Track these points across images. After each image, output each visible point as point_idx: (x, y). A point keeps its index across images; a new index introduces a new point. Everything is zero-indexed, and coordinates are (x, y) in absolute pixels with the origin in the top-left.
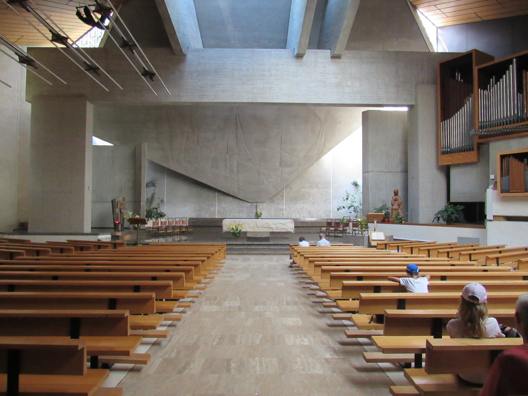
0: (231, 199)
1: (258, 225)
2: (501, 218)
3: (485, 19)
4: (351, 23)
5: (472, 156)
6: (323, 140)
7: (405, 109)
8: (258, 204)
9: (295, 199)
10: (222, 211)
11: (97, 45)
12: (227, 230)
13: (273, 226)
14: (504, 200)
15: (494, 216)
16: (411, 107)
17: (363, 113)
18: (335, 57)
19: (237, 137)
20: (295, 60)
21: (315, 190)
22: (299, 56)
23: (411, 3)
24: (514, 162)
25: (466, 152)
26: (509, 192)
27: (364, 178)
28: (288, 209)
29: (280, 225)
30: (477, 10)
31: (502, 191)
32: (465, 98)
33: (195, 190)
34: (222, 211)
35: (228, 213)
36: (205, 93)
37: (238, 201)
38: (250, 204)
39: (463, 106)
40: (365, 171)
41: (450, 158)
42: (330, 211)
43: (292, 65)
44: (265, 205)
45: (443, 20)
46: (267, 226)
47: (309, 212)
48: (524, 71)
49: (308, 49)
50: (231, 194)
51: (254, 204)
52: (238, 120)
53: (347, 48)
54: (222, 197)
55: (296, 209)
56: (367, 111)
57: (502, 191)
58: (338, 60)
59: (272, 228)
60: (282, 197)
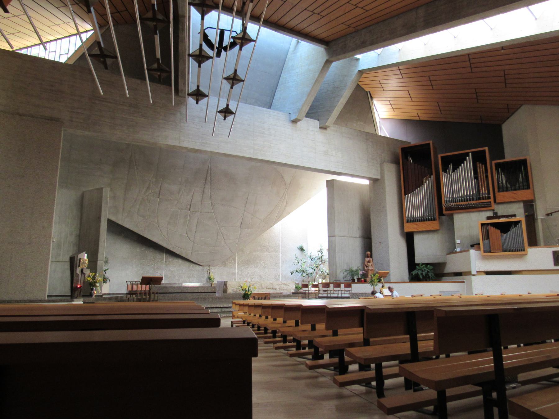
0: (180, 261)
1: (263, 285)
2: (483, 273)
3: (421, 119)
4: (345, 102)
5: (434, 225)
6: (285, 203)
7: (366, 182)
8: (211, 267)
9: (247, 263)
10: (169, 275)
11: (63, 60)
12: (232, 292)
13: (277, 287)
14: (484, 258)
15: (477, 272)
16: (374, 181)
17: (328, 182)
18: (323, 128)
19: (203, 192)
20: (291, 124)
21: (266, 253)
22: (295, 122)
23: (370, 95)
24: (492, 230)
25: (425, 222)
26: (490, 252)
27: (330, 243)
28: (240, 273)
29: (283, 286)
30: (419, 111)
31: (485, 252)
32: (423, 178)
33: (138, 250)
34: (169, 275)
35: (177, 278)
36: (208, 142)
37: (187, 264)
38: (201, 268)
39: (422, 184)
40: (331, 235)
41: (415, 226)
42: (279, 276)
43: (288, 129)
44: (217, 268)
45: (388, 113)
46: (271, 287)
47: (260, 276)
48: (478, 163)
49: (306, 117)
50: (184, 255)
51: (206, 268)
52: (209, 175)
53: (334, 123)
54: (171, 259)
55: (248, 273)
56: (332, 181)
57: (485, 252)
58: (324, 131)
59: (276, 289)
60: (234, 260)
